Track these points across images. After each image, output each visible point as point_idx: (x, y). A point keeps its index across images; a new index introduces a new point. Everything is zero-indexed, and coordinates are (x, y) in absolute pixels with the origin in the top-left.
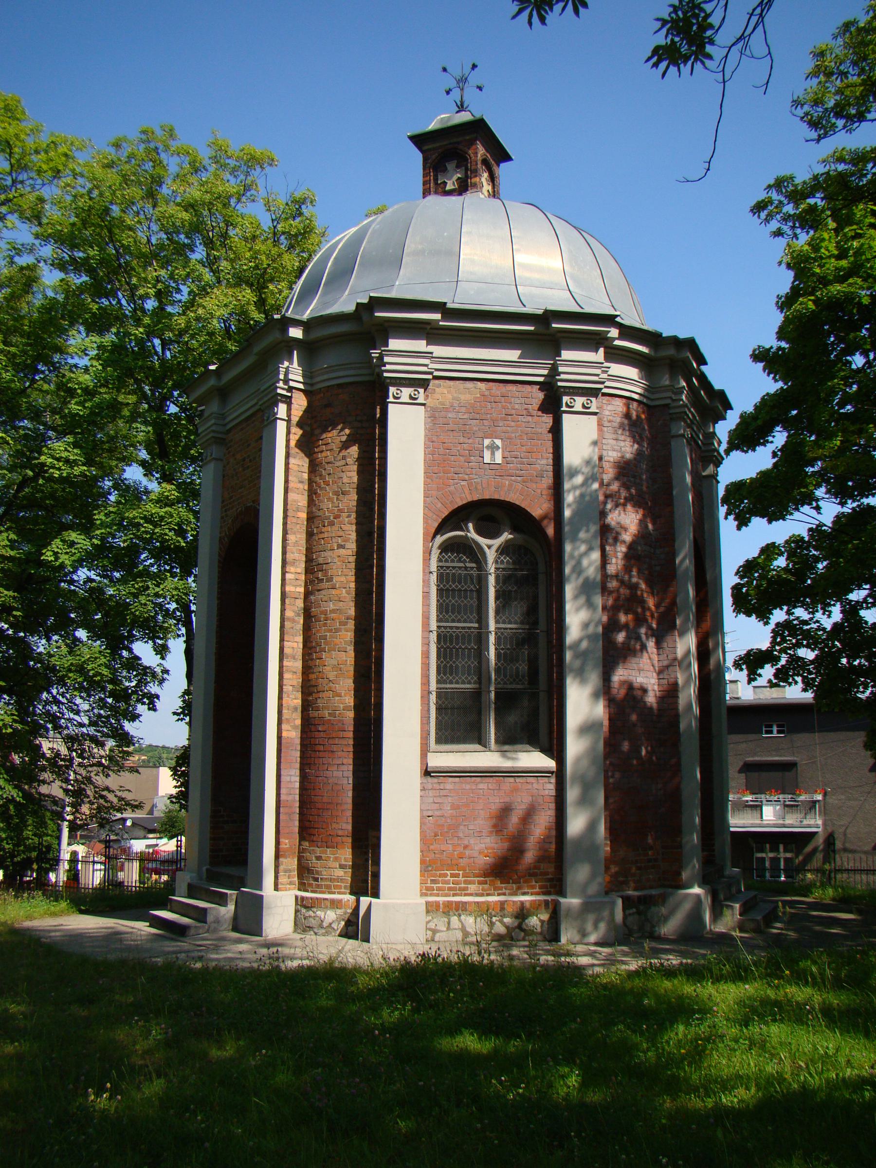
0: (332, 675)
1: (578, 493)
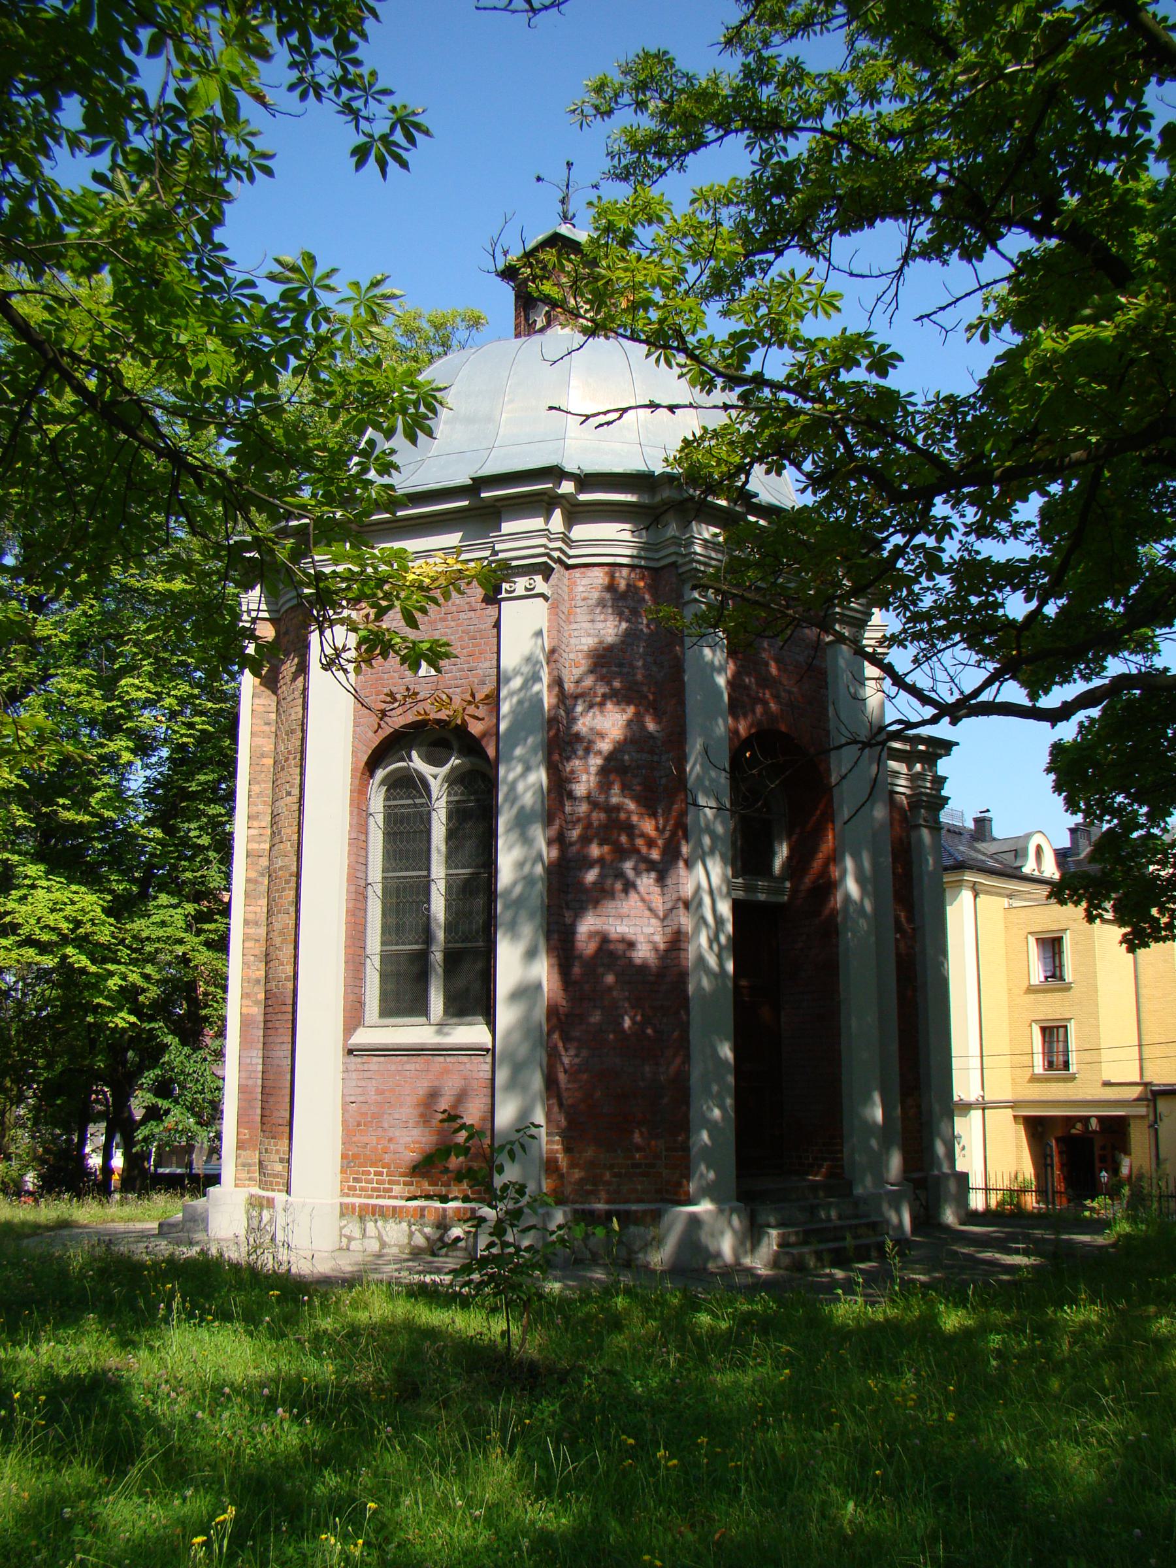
1: (515, 699)
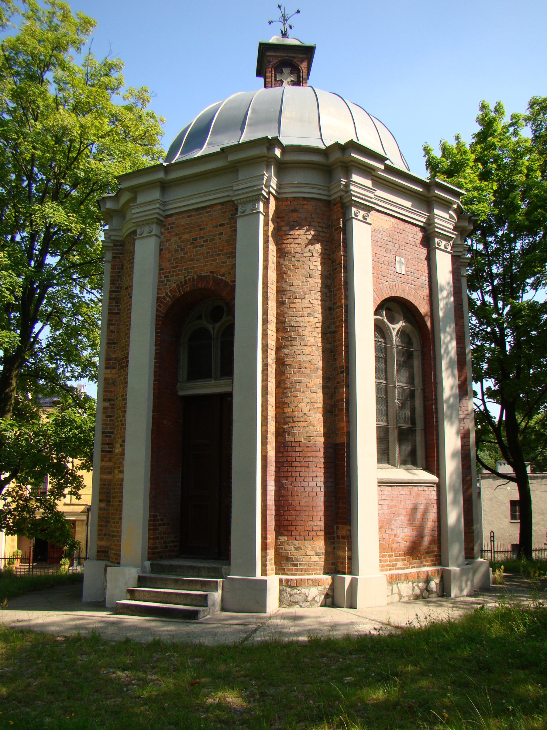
0: (306, 410)
1: (445, 302)
